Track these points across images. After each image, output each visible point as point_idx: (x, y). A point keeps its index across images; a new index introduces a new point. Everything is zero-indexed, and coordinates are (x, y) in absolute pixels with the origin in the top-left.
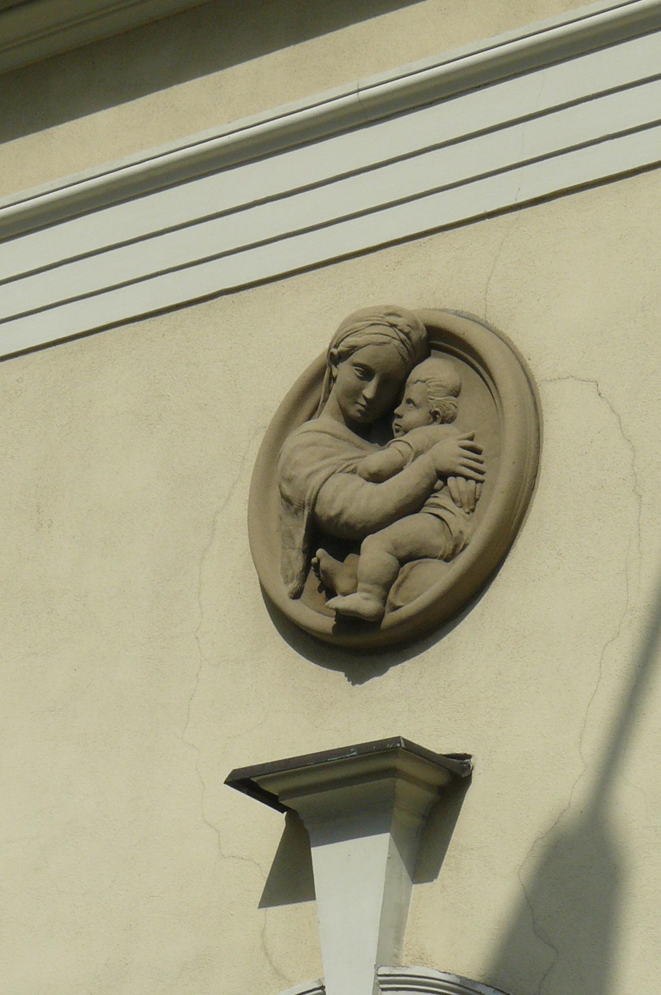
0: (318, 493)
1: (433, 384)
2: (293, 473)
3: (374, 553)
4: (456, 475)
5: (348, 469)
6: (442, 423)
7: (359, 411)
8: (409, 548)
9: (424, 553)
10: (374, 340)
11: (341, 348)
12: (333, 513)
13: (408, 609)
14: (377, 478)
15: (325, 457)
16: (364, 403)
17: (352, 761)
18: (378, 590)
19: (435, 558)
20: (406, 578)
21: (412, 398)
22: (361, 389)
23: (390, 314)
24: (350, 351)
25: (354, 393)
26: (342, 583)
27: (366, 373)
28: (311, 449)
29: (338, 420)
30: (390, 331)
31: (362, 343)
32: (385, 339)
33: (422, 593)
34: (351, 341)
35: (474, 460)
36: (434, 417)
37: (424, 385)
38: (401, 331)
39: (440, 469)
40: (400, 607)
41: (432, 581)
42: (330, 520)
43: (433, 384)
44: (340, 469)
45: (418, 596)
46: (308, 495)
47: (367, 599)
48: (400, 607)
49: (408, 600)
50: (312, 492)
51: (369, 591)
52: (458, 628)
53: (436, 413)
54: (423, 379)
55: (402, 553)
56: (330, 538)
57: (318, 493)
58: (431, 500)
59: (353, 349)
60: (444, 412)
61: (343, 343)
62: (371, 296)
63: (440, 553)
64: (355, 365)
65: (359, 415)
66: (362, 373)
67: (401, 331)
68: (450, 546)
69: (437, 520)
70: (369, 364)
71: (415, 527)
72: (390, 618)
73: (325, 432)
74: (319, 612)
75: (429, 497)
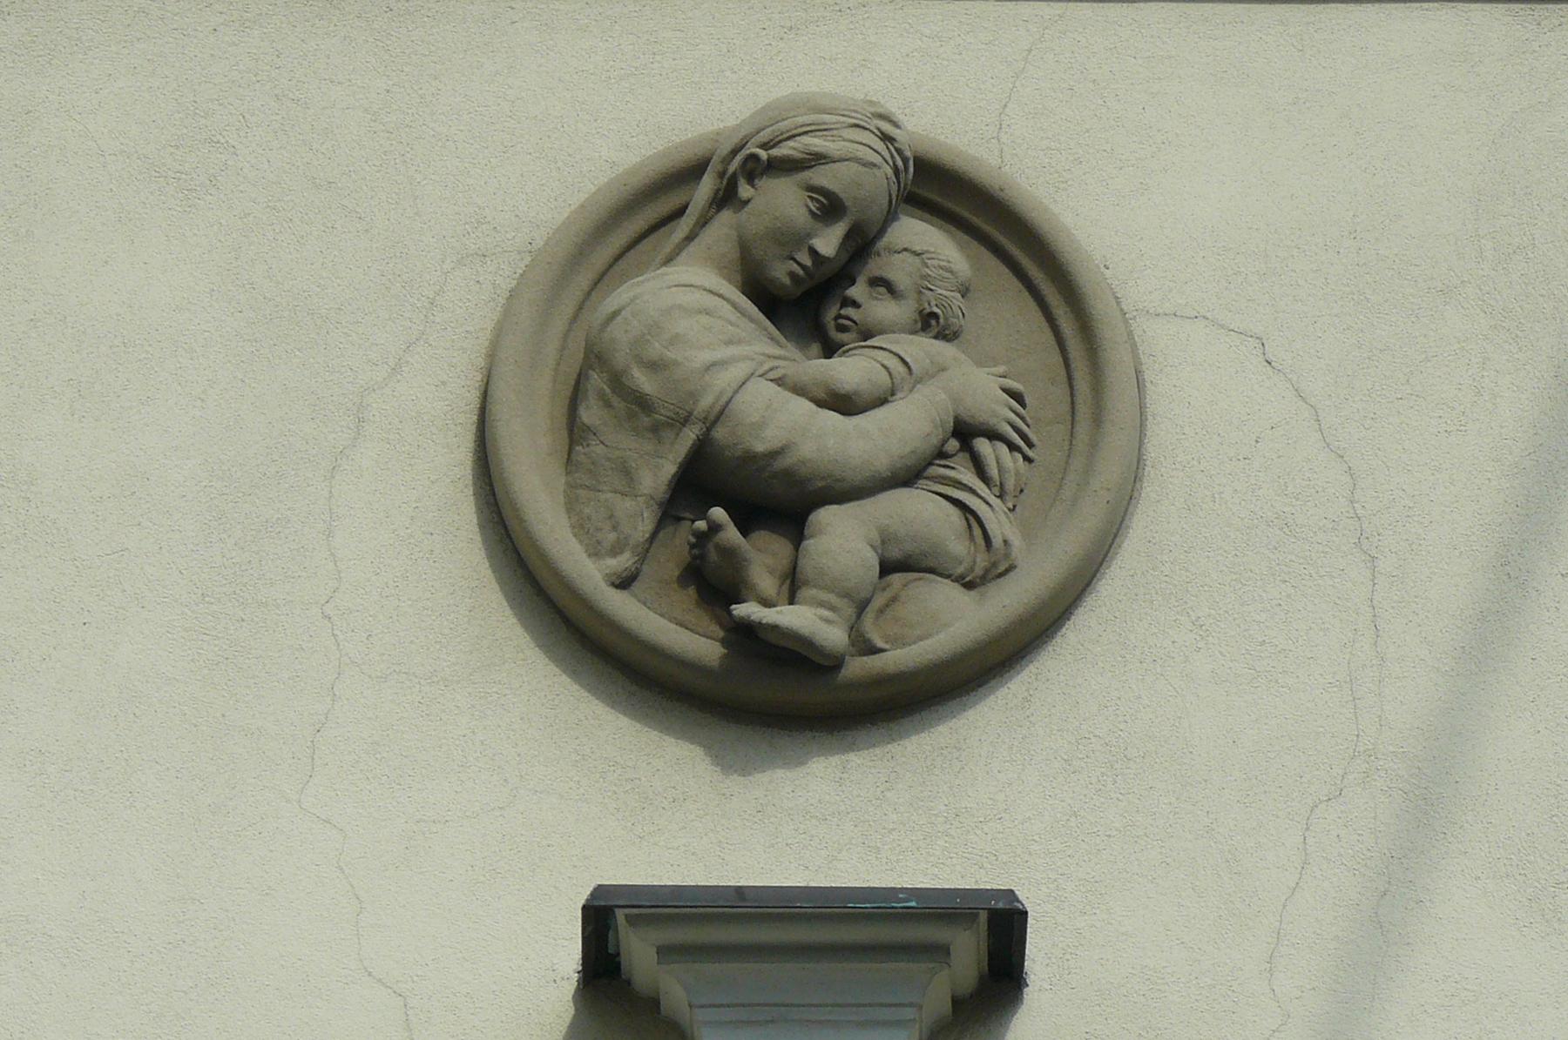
0: (728, 403)
1: (935, 262)
2: (671, 354)
3: (842, 539)
4: (994, 436)
5: (772, 375)
6: (936, 337)
7: (792, 275)
8: (909, 547)
9: (931, 563)
10: (860, 155)
11: (775, 152)
12: (760, 447)
13: (897, 658)
14: (844, 403)
15: (729, 343)
16: (808, 262)
17: (908, 916)
18: (849, 611)
19: (948, 577)
20: (894, 599)
21: (891, 275)
22: (809, 236)
23: (881, 117)
24: (802, 161)
25: (789, 240)
26: (763, 577)
27: (829, 207)
28: (704, 319)
29: (730, 281)
30: (879, 145)
31: (836, 154)
32: (877, 159)
33: (928, 636)
34: (816, 143)
35: (1018, 415)
36: (927, 322)
37: (917, 260)
38: (899, 151)
39: (965, 416)
40: (882, 650)
41: (948, 620)
42: (750, 458)
43: (935, 262)
44: (761, 371)
45: (921, 638)
46: (706, 402)
47: (827, 621)
48: (882, 650)
49: (899, 642)
50: (717, 399)
51: (832, 608)
52: (971, 714)
53: (934, 315)
54: (917, 248)
55: (895, 553)
56: (737, 496)
57: (728, 403)
58: (935, 470)
59: (818, 159)
60: (946, 319)
61: (791, 143)
62: (728, 73)
63: (960, 570)
64: (811, 189)
65: (787, 281)
66: (822, 207)
67: (899, 151)
68: (982, 561)
69: (954, 513)
70: (842, 195)
71: (921, 513)
72: (857, 667)
73: (720, 296)
74: (681, 625)
75: (931, 464)
